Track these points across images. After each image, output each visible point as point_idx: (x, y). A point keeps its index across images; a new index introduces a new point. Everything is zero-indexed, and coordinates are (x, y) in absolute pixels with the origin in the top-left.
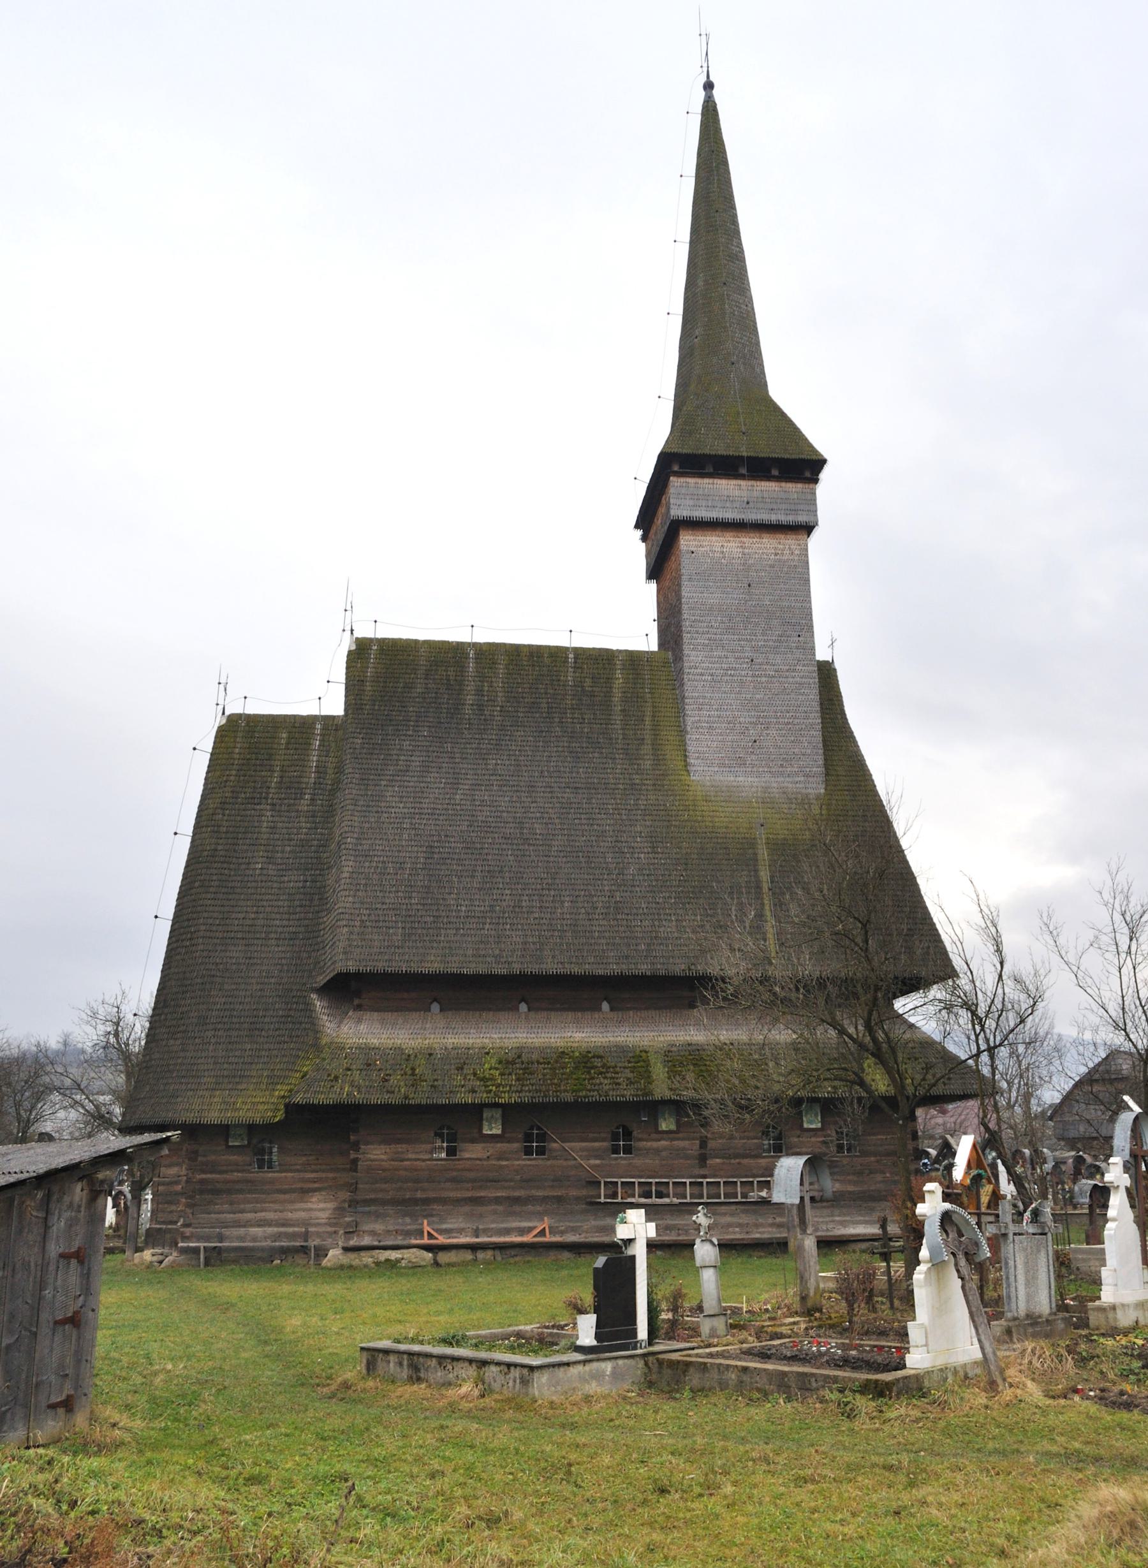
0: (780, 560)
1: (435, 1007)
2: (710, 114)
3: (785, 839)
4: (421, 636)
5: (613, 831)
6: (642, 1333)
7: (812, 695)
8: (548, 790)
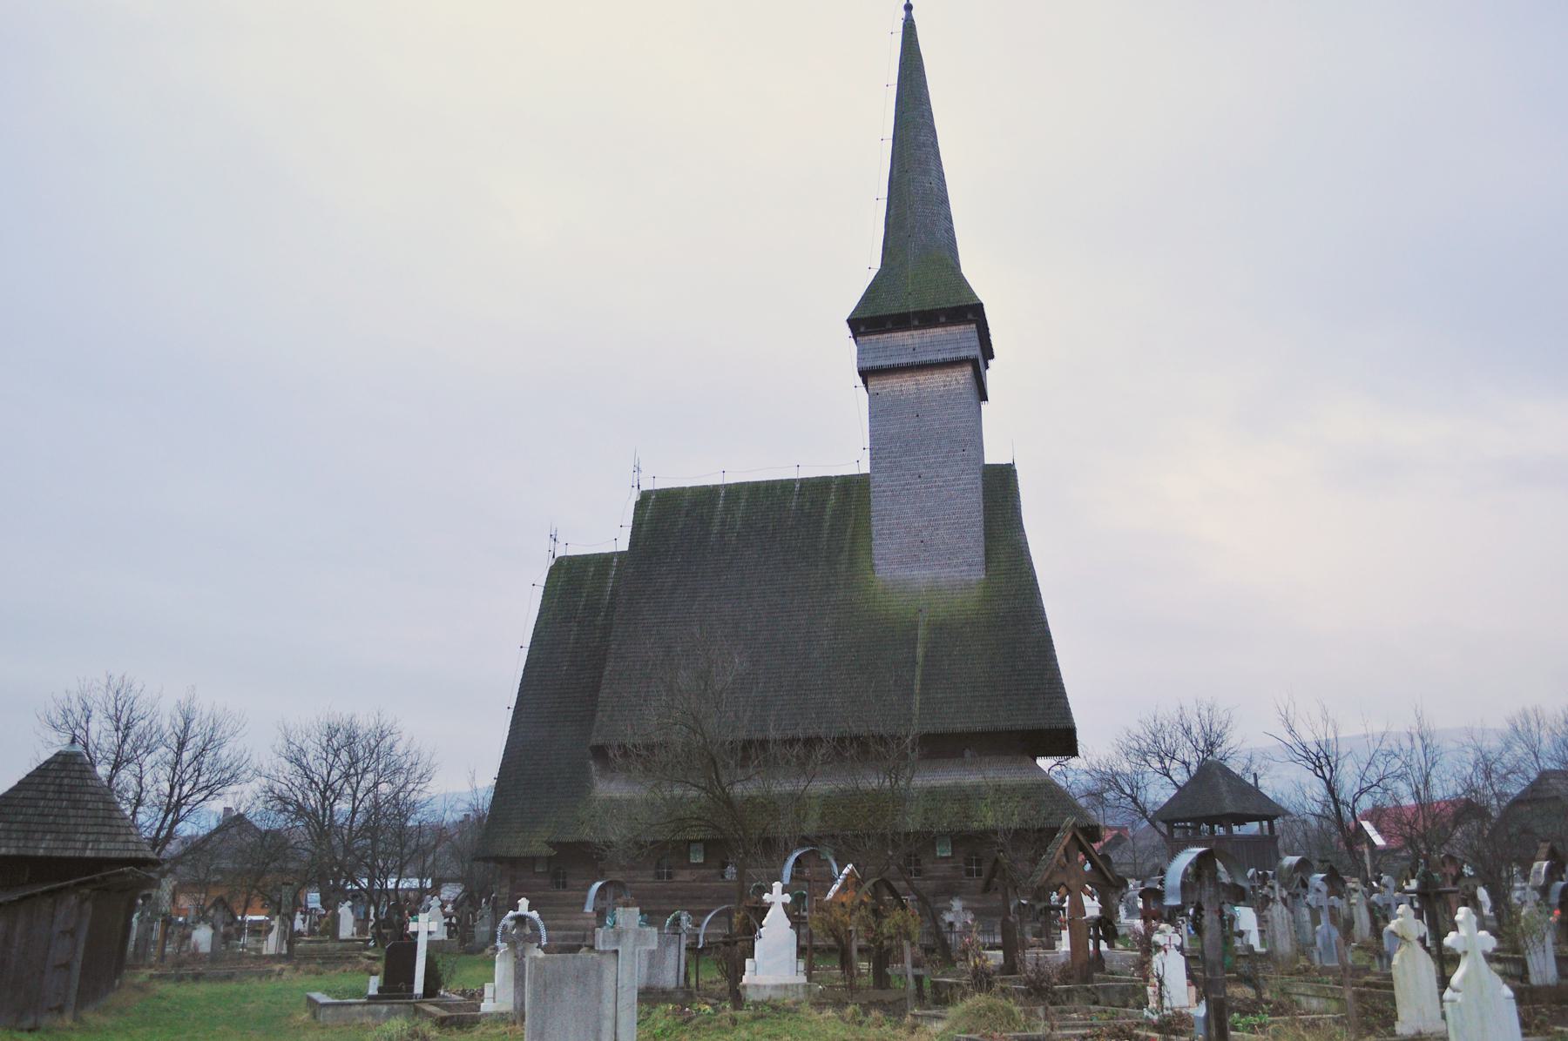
0: (948, 390)
1: (968, 753)
2: (909, 29)
3: (945, 620)
4: (688, 484)
5: (807, 624)
6: (419, 988)
7: (972, 502)
8: (762, 595)
